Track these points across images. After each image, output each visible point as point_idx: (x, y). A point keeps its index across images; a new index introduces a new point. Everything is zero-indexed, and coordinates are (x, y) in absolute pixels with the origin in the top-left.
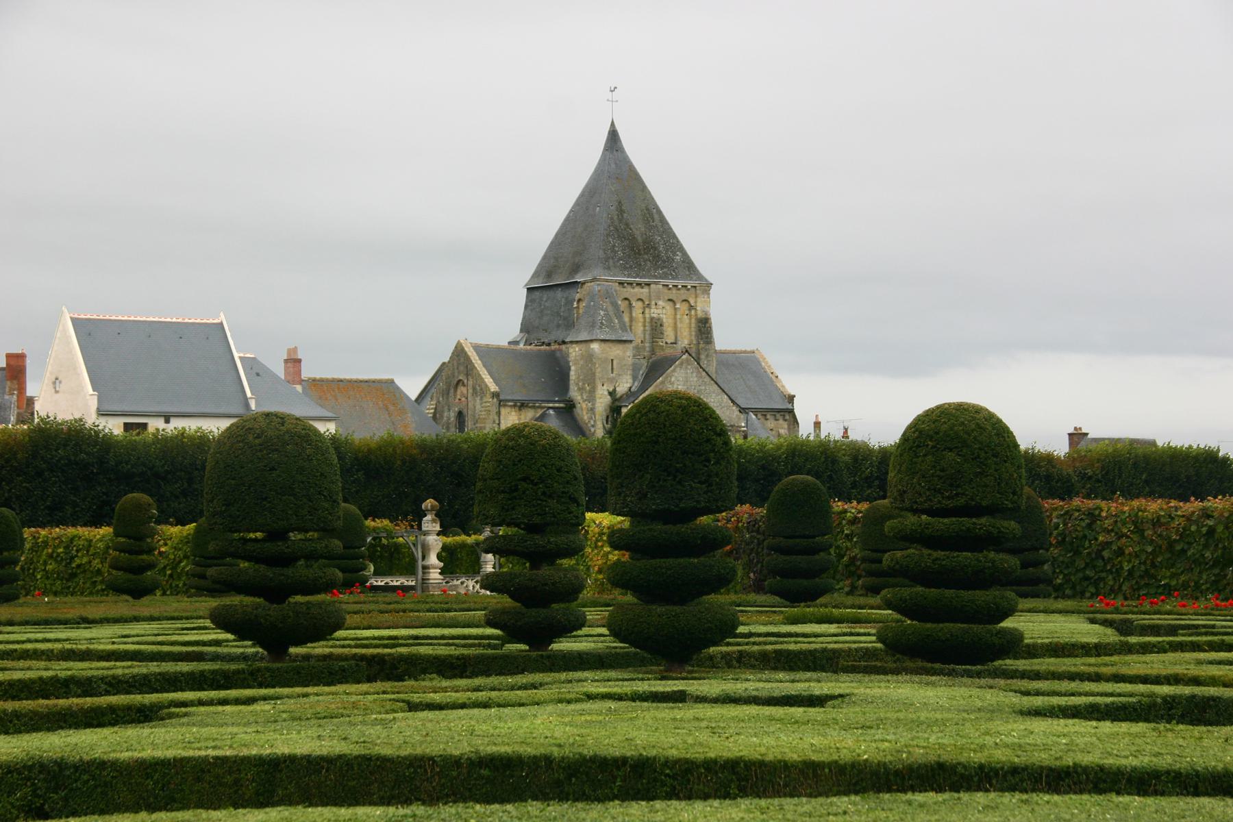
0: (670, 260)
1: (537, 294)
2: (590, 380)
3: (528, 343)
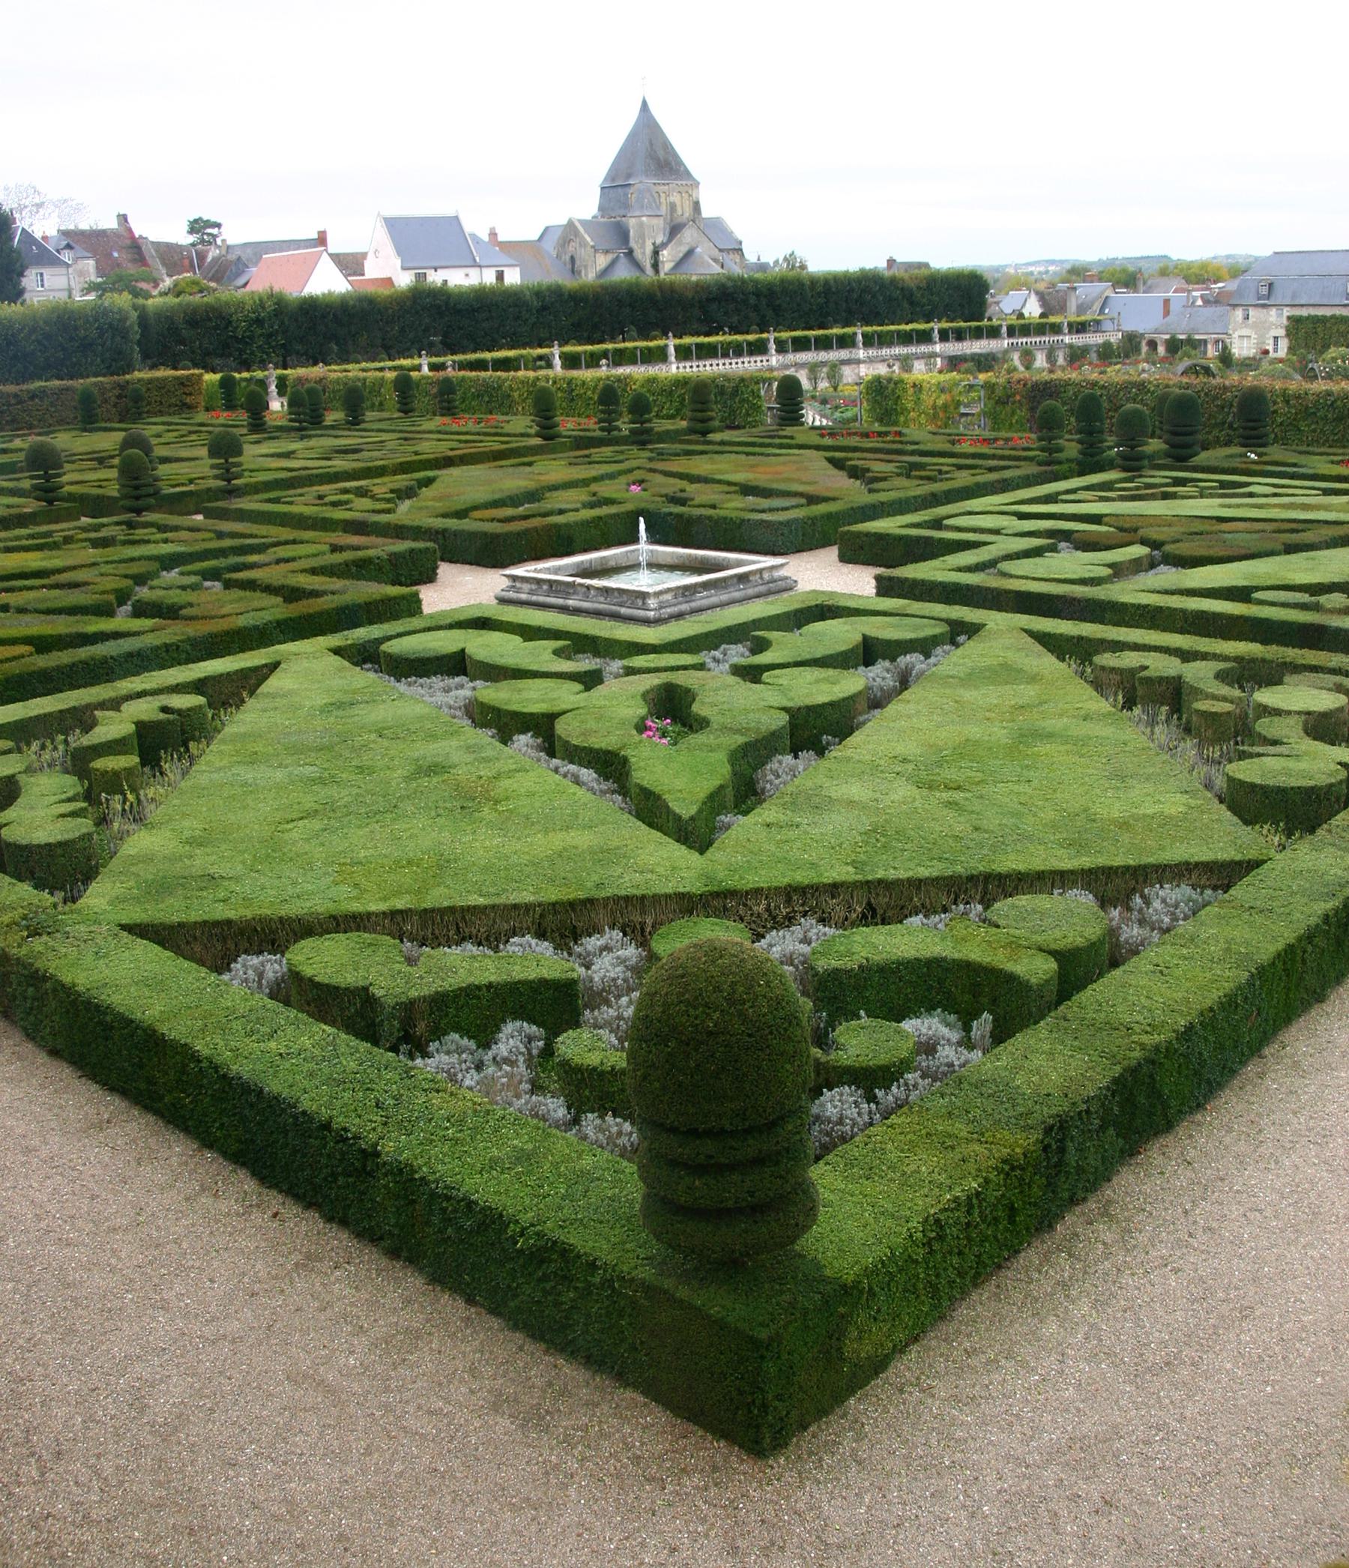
0: (678, 171)
1: (606, 190)
2: (642, 237)
3: (602, 217)
